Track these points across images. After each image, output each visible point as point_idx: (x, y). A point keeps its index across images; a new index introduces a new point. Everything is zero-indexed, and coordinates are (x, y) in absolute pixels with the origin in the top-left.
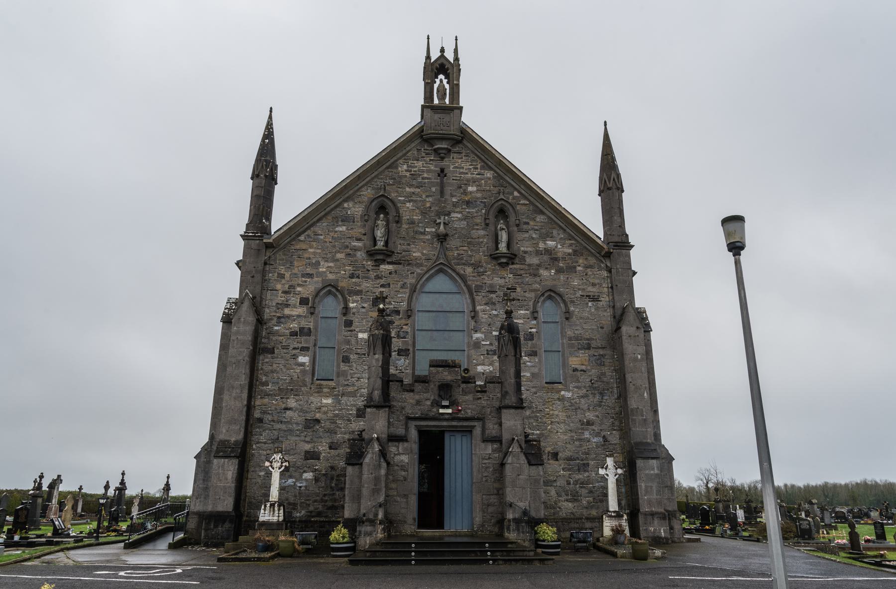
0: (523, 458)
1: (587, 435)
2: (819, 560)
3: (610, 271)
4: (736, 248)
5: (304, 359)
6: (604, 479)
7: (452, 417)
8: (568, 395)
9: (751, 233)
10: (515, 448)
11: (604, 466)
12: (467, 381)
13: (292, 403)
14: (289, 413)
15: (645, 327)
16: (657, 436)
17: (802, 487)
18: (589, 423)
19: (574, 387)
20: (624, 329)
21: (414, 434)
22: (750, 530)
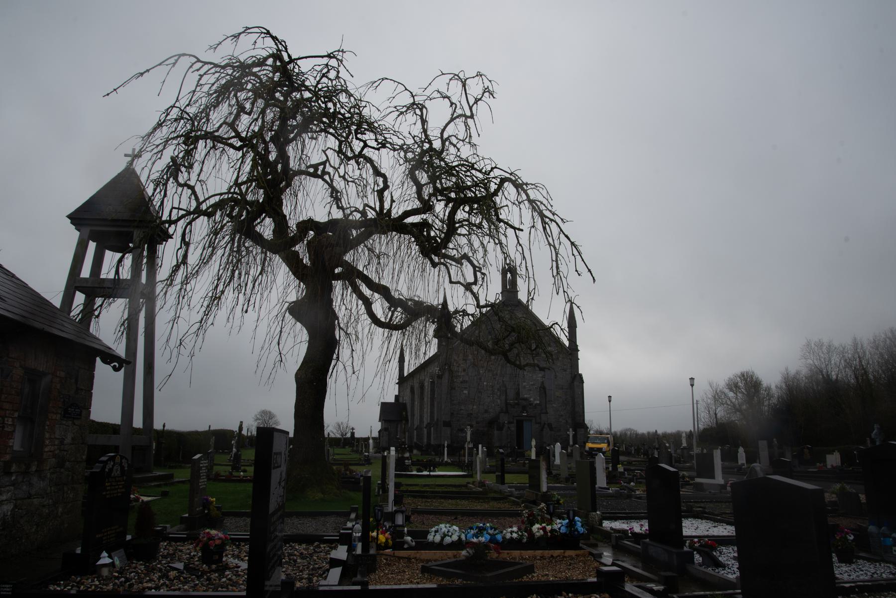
0: (548, 429)
1: (561, 420)
2: (335, 371)
3: (571, 360)
4: (610, 401)
5: (465, 392)
6: (569, 435)
7: (526, 416)
8: (555, 406)
9: (612, 399)
10: (546, 426)
11: (568, 430)
12: (531, 404)
13: (463, 408)
14: (462, 411)
15: (582, 381)
16: (584, 420)
17: (619, 433)
18: (562, 416)
19: (724, 566)
20: (575, 383)
21: (515, 421)
22: (602, 441)
